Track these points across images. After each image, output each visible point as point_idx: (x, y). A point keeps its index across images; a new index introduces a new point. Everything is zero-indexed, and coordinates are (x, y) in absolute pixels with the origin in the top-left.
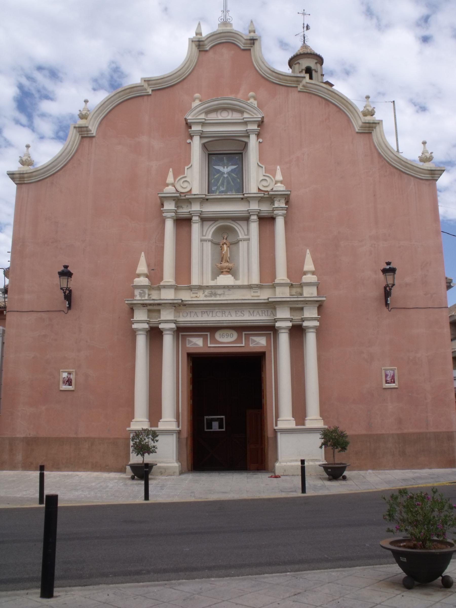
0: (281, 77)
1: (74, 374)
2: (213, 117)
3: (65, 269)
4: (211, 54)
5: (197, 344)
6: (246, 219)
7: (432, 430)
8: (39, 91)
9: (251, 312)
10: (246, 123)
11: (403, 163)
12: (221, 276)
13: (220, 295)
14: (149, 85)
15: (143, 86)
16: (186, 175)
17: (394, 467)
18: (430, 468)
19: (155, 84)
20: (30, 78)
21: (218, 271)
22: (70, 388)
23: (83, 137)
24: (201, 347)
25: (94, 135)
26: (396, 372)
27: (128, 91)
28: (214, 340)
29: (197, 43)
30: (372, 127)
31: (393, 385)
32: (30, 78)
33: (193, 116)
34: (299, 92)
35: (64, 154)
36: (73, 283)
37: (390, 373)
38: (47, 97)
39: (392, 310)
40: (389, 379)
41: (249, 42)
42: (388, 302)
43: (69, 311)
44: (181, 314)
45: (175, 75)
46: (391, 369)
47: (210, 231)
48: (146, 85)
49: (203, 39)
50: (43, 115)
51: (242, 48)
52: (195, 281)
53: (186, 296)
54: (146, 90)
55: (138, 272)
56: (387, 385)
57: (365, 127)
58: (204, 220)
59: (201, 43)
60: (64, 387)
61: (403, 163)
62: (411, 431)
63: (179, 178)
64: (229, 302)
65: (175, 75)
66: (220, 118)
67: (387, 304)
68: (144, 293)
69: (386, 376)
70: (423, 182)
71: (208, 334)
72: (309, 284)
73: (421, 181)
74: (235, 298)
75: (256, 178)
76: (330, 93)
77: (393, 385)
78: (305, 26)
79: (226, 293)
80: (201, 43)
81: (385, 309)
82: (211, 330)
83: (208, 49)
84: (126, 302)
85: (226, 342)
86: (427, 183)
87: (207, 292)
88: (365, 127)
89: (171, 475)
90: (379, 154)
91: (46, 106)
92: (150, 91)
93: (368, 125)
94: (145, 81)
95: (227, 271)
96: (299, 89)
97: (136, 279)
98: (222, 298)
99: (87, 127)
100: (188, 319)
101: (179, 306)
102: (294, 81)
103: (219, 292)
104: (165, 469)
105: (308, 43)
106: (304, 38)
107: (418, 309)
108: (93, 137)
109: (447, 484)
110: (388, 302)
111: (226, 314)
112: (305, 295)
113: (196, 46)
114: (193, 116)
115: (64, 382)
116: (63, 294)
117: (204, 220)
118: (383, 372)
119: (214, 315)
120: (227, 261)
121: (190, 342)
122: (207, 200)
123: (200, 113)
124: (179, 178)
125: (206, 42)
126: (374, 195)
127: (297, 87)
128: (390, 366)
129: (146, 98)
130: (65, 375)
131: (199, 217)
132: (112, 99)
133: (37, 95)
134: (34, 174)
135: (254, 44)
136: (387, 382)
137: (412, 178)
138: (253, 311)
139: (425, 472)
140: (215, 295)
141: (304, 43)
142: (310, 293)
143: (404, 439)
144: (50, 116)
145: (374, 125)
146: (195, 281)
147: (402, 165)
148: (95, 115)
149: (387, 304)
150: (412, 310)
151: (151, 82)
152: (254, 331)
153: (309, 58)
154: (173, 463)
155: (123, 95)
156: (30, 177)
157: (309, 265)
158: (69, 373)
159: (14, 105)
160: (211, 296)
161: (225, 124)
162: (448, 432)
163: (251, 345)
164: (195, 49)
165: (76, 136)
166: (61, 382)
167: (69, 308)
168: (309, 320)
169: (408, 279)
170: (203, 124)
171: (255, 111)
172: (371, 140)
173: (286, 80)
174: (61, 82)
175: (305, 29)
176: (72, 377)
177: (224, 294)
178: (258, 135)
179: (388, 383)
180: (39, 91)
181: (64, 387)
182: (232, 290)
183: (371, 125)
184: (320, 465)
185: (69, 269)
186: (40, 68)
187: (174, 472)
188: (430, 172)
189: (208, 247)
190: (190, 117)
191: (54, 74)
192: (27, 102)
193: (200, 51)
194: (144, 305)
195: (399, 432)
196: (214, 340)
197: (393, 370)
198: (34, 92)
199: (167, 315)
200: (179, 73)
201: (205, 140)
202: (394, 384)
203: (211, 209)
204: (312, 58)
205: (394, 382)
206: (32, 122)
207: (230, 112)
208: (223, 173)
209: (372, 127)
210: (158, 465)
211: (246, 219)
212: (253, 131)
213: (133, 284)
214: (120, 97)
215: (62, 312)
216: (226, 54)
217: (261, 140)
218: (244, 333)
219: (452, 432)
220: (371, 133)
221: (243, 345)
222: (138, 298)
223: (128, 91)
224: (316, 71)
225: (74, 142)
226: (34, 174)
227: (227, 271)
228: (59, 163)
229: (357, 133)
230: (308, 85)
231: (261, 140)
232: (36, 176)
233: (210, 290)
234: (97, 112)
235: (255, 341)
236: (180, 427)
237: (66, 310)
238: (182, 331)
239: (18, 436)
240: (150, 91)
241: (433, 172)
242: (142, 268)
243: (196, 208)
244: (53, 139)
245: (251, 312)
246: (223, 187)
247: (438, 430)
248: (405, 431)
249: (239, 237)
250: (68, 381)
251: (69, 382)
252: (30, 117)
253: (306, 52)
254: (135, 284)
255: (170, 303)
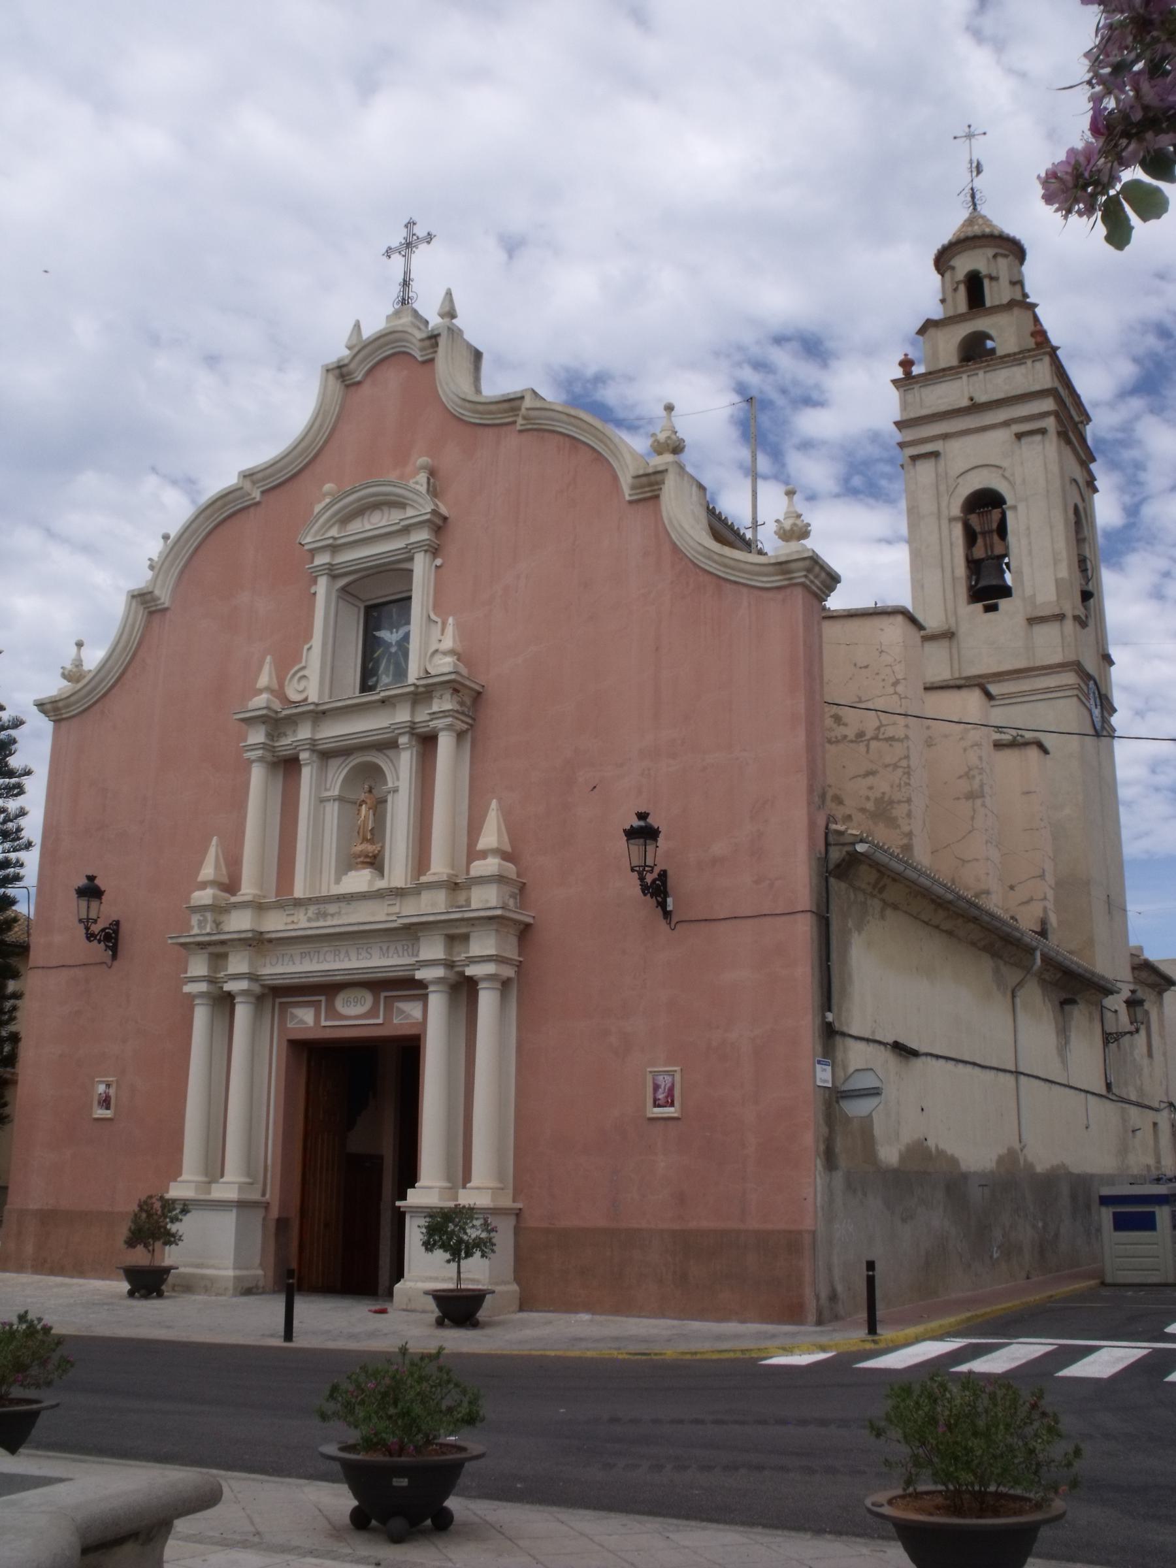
0: (480, 408)
1: (114, 1085)
2: (359, 527)
3: (642, 823)
4: (366, 389)
5: (306, 1020)
6: (388, 745)
7: (753, 1224)
8: (784, 391)
9: (385, 948)
10: (406, 530)
11: (716, 557)
12: (353, 873)
13: (332, 915)
14: (254, 483)
15: (241, 488)
16: (303, 664)
17: (661, 1313)
18: (743, 1321)
19: (264, 479)
20: (760, 365)
21: (349, 863)
22: (108, 1114)
23: (151, 613)
24: (310, 1028)
25: (166, 605)
26: (678, 1077)
27: (219, 503)
28: (332, 1013)
29: (337, 372)
30: (657, 483)
31: (669, 1111)
32: (760, 365)
33: (315, 536)
34: (521, 431)
35: (115, 653)
36: (661, 853)
37: (664, 1081)
38: (810, 400)
39: (678, 926)
40: (661, 1096)
41: (427, 343)
42: (669, 909)
43: (115, 963)
44: (268, 961)
45: (295, 453)
46: (669, 1073)
47: (338, 773)
48: (248, 485)
49: (346, 361)
50: (806, 445)
51: (420, 359)
52: (299, 892)
53: (275, 923)
54: (249, 494)
55: (201, 878)
56: (657, 1110)
57: (642, 487)
58: (326, 755)
59: (345, 370)
60: (100, 1113)
61: (716, 557)
62: (705, 1224)
63: (292, 672)
64: (355, 928)
65: (295, 453)
66: (368, 527)
67: (667, 914)
68: (205, 920)
69: (656, 1087)
70: (770, 595)
71: (323, 998)
72: (482, 880)
73: (766, 595)
74: (361, 920)
75: (430, 644)
76: (573, 420)
77: (669, 1111)
78: (974, 165)
79: (343, 911)
80: (345, 370)
81: (662, 924)
82: (326, 990)
83: (359, 379)
84: (170, 941)
85: (354, 1016)
86: (780, 596)
87: (312, 909)
88: (642, 487)
89: (221, 1295)
90: (674, 545)
91: (812, 423)
92: (257, 495)
93: (644, 480)
94: (245, 476)
95: (363, 863)
96: (519, 427)
97: (197, 894)
98: (335, 922)
99: (151, 593)
100: (347, 965)
101: (258, 942)
102: (505, 411)
103: (332, 908)
104: (212, 1280)
105: (984, 210)
106: (973, 196)
107: (738, 921)
108: (166, 609)
109: (620, 1357)
110: (669, 909)
111: (342, 956)
112: (473, 906)
113: (337, 378)
114: (315, 536)
115: (99, 1103)
116: (638, 882)
117: (326, 755)
118: (649, 1078)
119: (321, 958)
120: (368, 841)
121: (294, 1016)
122: (324, 712)
123: (328, 525)
124: (292, 672)
125: (352, 366)
126: (657, 649)
127: (514, 422)
128: (665, 1066)
129: (252, 510)
130: (101, 1088)
131: (313, 751)
132: (194, 526)
133: (780, 401)
134: (73, 699)
135: (437, 345)
136: (656, 1104)
137: (745, 590)
138: (388, 948)
139: (731, 1327)
140: (325, 915)
141: (975, 209)
142: (486, 899)
143: (687, 1244)
144: (824, 443)
145: (658, 477)
146: (299, 892)
147: (715, 562)
148: (166, 564)
149: (667, 914)
150: (723, 922)
151: (255, 477)
152: (305, 996)
153: (975, 248)
154: (226, 1269)
155: (212, 516)
156: (67, 706)
157: (489, 838)
158: (108, 1086)
159: (734, 433)
160: (317, 919)
161: (372, 540)
162: (790, 1232)
163: (289, 1026)
164: (334, 385)
165: (136, 613)
166: (95, 1103)
167: (114, 957)
168: (479, 962)
169: (718, 848)
170: (334, 548)
171: (420, 500)
172: (657, 512)
173: (491, 413)
174: (838, 358)
175: (975, 174)
176: (112, 1092)
177: (339, 913)
178: (434, 551)
179: (659, 1106)
180: (784, 391)
181: (100, 1113)
182: (354, 904)
183: (653, 478)
184: (427, 1293)
185: (97, 882)
186: (779, 340)
187: (226, 1289)
188: (777, 567)
189: (332, 811)
190: (308, 540)
191: (813, 347)
192: (764, 419)
193: (347, 386)
194: (202, 945)
195: (676, 1226)
196: (332, 1013)
197: (671, 1074)
198: (774, 395)
199: (238, 964)
200: (303, 445)
201: (342, 582)
202: (672, 1109)
203: (334, 731)
204: (981, 247)
205: (672, 1105)
206: (783, 465)
207: (386, 509)
208: (390, 645)
209: (657, 483)
210: (182, 1270)
211: (388, 745)
212: (418, 546)
213: (189, 902)
214: (207, 519)
215: (104, 966)
216: (393, 379)
217: (438, 562)
218: (383, 994)
219: (800, 1232)
220: (657, 497)
221: (380, 1021)
222: (196, 931)
223: (219, 503)
224: (992, 278)
225: (133, 626)
226: (73, 699)
227: (363, 863)
228: (109, 672)
229: (630, 502)
230: (536, 413)
231: (438, 562)
232: (77, 702)
233: (316, 907)
234: (170, 558)
235: (403, 1012)
236: (268, 1196)
237: (109, 962)
238: (277, 995)
239: (31, 1207)
240: (257, 495)
241: (784, 566)
242: (208, 871)
243: (304, 733)
244: (837, 496)
245: (385, 948)
246: (388, 676)
247: (769, 1227)
248: (693, 1225)
249: (386, 783)
250: (105, 1101)
251: (106, 1102)
252: (777, 455)
253: (970, 234)
254: (193, 903)
255: (240, 940)
